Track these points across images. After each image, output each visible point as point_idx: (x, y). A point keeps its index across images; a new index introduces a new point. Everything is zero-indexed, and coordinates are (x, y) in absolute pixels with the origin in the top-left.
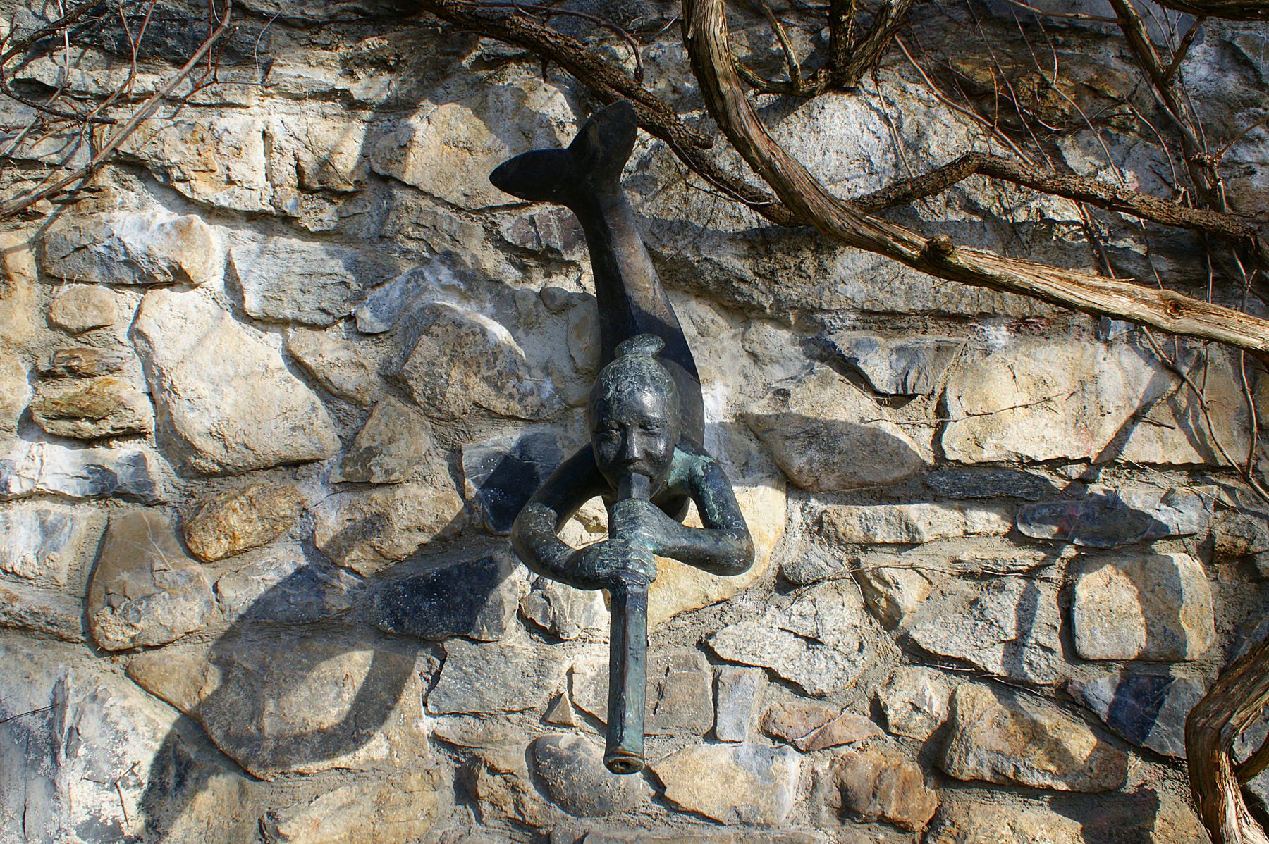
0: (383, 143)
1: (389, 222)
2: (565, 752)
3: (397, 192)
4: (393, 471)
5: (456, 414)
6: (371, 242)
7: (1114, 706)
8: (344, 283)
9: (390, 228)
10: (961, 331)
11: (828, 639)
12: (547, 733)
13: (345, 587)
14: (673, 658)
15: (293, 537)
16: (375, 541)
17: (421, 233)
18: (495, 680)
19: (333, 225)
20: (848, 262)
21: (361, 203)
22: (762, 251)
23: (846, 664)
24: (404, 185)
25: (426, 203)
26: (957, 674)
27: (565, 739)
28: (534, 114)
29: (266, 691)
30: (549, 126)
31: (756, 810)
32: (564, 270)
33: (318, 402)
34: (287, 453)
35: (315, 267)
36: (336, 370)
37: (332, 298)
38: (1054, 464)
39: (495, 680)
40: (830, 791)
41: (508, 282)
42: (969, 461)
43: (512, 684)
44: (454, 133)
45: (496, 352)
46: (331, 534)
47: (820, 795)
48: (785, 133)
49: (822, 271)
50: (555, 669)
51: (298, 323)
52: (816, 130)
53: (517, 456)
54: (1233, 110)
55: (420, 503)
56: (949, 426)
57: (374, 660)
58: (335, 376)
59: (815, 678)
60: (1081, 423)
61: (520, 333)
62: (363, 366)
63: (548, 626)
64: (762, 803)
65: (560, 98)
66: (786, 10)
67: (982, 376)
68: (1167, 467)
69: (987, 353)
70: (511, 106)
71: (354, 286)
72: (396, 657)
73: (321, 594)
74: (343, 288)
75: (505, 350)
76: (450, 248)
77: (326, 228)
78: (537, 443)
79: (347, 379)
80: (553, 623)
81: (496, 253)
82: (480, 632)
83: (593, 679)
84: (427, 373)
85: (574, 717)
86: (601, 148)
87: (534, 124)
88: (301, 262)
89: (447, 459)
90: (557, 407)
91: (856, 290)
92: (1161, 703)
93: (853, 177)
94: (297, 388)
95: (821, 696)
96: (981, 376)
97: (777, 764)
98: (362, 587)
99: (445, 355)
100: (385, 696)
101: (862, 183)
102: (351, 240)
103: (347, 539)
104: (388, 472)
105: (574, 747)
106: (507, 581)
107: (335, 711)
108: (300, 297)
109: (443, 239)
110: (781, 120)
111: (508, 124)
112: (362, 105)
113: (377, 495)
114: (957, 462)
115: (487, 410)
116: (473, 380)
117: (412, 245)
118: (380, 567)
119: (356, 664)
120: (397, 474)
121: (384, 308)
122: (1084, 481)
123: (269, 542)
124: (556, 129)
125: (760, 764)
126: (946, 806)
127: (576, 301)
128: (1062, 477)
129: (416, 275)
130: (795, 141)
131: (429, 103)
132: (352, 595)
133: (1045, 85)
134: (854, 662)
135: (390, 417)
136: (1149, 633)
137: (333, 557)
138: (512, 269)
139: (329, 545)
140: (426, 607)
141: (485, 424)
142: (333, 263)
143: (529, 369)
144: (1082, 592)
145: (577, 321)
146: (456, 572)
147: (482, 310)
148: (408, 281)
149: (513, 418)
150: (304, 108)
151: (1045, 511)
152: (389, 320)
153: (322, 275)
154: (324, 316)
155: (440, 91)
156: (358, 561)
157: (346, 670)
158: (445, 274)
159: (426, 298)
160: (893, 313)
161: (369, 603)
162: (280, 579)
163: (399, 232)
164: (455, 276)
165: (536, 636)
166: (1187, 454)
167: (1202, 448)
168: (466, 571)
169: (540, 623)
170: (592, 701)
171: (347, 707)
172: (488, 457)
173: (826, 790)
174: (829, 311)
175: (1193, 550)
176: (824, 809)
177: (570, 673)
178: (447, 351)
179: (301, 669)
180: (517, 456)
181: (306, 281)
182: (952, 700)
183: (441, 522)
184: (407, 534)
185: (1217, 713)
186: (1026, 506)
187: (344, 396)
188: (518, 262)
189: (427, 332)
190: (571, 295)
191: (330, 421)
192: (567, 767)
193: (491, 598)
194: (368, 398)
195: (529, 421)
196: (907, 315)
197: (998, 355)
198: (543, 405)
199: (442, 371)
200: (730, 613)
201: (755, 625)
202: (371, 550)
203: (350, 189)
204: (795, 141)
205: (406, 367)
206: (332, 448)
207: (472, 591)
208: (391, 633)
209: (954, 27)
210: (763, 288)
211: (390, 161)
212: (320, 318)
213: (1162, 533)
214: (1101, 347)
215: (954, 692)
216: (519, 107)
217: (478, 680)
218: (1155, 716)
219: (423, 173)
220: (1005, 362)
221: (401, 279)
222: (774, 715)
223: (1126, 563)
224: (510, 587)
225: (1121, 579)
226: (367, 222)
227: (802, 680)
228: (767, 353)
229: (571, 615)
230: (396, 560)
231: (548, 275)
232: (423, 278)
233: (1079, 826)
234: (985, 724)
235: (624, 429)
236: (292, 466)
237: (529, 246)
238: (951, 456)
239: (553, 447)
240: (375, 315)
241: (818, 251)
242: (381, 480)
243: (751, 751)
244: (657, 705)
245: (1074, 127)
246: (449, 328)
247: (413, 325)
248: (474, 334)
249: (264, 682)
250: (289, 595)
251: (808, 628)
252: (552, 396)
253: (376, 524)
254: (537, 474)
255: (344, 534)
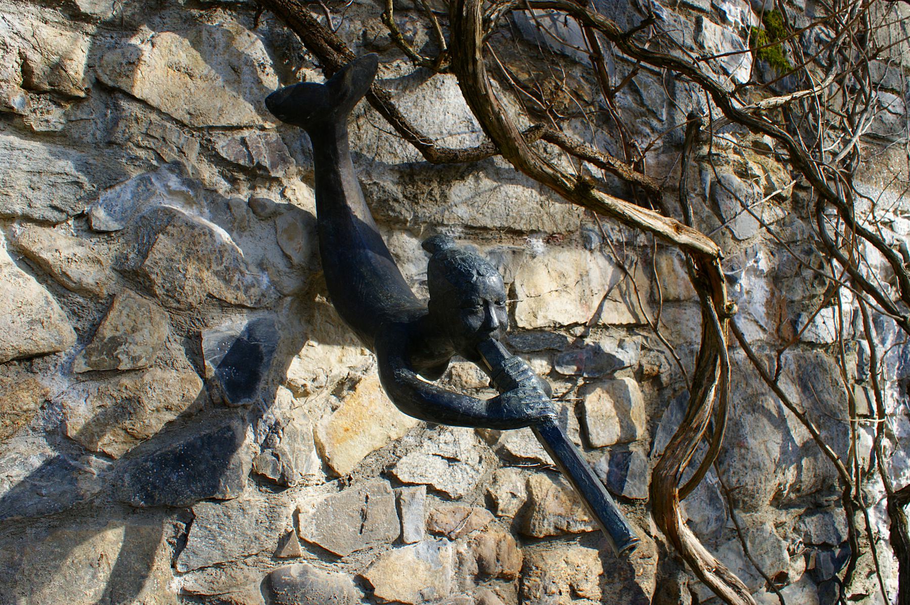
0: (110, 57)
1: (119, 130)
2: (298, 579)
3: (124, 104)
4: (140, 358)
5: (194, 304)
6: (97, 146)
7: (609, 474)
8: (77, 183)
9: (120, 135)
10: (519, 242)
11: (462, 457)
12: (277, 568)
13: (95, 472)
14: (370, 488)
15: (34, 429)
16: (127, 423)
17: (151, 143)
18: (234, 531)
19: (60, 127)
20: (457, 192)
21: (86, 109)
22: (407, 180)
23: (474, 473)
24: (133, 98)
25: (154, 117)
26: (528, 468)
27: (293, 569)
28: (240, 54)
29: (18, 589)
30: (253, 65)
31: (433, 588)
32: (267, 185)
33: (50, 297)
34: (27, 347)
35: (41, 165)
36: (73, 265)
37: (64, 195)
38: (569, 327)
39: (234, 531)
40: (472, 564)
41: (221, 192)
42: (529, 327)
43: (248, 532)
44: (176, 59)
45: (222, 251)
46: (82, 422)
47: (465, 568)
48: (420, 96)
49: (444, 197)
50: (285, 513)
51: (27, 219)
52: (440, 97)
53: (245, 338)
54: (636, 117)
55: (167, 385)
56: (519, 305)
57: (126, 535)
58: (76, 271)
59: (456, 486)
60: (583, 300)
61: (235, 234)
62: (99, 262)
63: (277, 478)
64: (437, 583)
65: (260, 44)
66: (411, 9)
67: (532, 271)
68: (621, 326)
69: (533, 257)
70: (222, 45)
71: (87, 186)
72: (146, 529)
73: (73, 481)
74: (75, 188)
75: (229, 249)
76: (178, 159)
77: (52, 129)
78: (260, 327)
79: (87, 275)
80: (283, 475)
81: (210, 166)
82: (224, 493)
83: (314, 515)
84: (166, 269)
85: (302, 550)
86: (351, 88)
87: (241, 62)
88: (24, 160)
89: (183, 344)
90: (273, 296)
91: (463, 212)
92: (628, 468)
93: (462, 133)
94: (29, 283)
95: (460, 498)
96: (532, 271)
97: (442, 552)
98: (110, 468)
99: (182, 251)
100: (138, 566)
101: (467, 138)
102: (75, 143)
103: (99, 425)
104: (134, 359)
105: (304, 572)
106: (244, 445)
107: (91, 593)
108: (29, 193)
109: (172, 149)
110: (417, 86)
111: (220, 59)
112: (87, 18)
113: (126, 381)
114: (523, 328)
115: (219, 300)
116: (206, 274)
117: (141, 153)
118: (129, 448)
119: (110, 542)
120: (144, 360)
121: (117, 208)
122: (583, 336)
123: (8, 437)
124: (258, 69)
125: (432, 555)
126: (528, 557)
127: (282, 210)
128: (572, 335)
129: (144, 180)
130: (427, 103)
131: (147, 29)
132: (102, 478)
133: (558, 87)
134: (478, 471)
135: (131, 308)
136: (621, 426)
137: (86, 444)
138: (223, 182)
139: (81, 433)
140: (174, 478)
141: (216, 312)
142: (62, 163)
143: (247, 264)
144: (588, 406)
145: (286, 226)
146: (199, 443)
147: (201, 214)
148: (138, 185)
149: (241, 306)
150: (22, 10)
151: (568, 357)
152: (122, 219)
153: (52, 173)
154: (56, 213)
155: (157, 20)
156: (109, 445)
157: (100, 550)
158: (174, 182)
159: (154, 201)
160: (485, 229)
161: (119, 483)
162: (27, 474)
163: (129, 139)
164: (183, 183)
165: (264, 488)
166: (628, 319)
167: (635, 315)
168: (209, 440)
169: (271, 477)
170: (315, 533)
171: (103, 586)
172: (223, 340)
173: (469, 564)
174: (447, 226)
175: (632, 374)
176: (468, 577)
177: (297, 512)
178: (184, 249)
179: (55, 559)
180: (245, 338)
181: (35, 179)
182: (528, 486)
183: (188, 400)
184: (155, 414)
185: (672, 466)
186: (559, 354)
187: (81, 290)
188: (229, 175)
189: (163, 231)
190: (278, 205)
191: (64, 314)
192: (303, 590)
193: (232, 461)
194: (105, 292)
195: (252, 309)
196: (491, 230)
197: (540, 257)
198: (263, 295)
199: (181, 266)
200: (399, 448)
201: (418, 454)
202: (122, 433)
203: (82, 94)
204: (427, 103)
205: (147, 262)
206: (70, 339)
207: (214, 458)
208: (142, 508)
209: (504, 41)
210: (407, 206)
211: (120, 74)
212: (52, 215)
213: (621, 366)
214: (588, 252)
215: (528, 482)
216: (228, 46)
217: (220, 534)
218: (626, 476)
219: (151, 90)
220: (543, 262)
221: (131, 183)
222: (435, 518)
223: (606, 386)
224: (246, 450)
225: (605, 396)
226: (91, 128)
227: (449, 489)
228: (406, 254)
229: (297, 467)
230: (146, 440)
231: (253, 188)
232: (151, 183)
233: (597, 551)
234: (550, 498)
235: (486, 304)
236: (28, 360)
237: (242, 162)
238: (520, 325)
239: (273, 330)
240: (109, 214)
241: (440, 183)
242: (128, 367)
243: (425, 547)
244: (362, 526)
245: (571, 115)
246: (184, 229)
247: (147, 228)
248: (205, 234)
249: (16, 581)
250: (41, 487)
251: (449, 451)
252: (268, 287)
253: (128, 407)
254: (260, 353)
255: (96, 421)
